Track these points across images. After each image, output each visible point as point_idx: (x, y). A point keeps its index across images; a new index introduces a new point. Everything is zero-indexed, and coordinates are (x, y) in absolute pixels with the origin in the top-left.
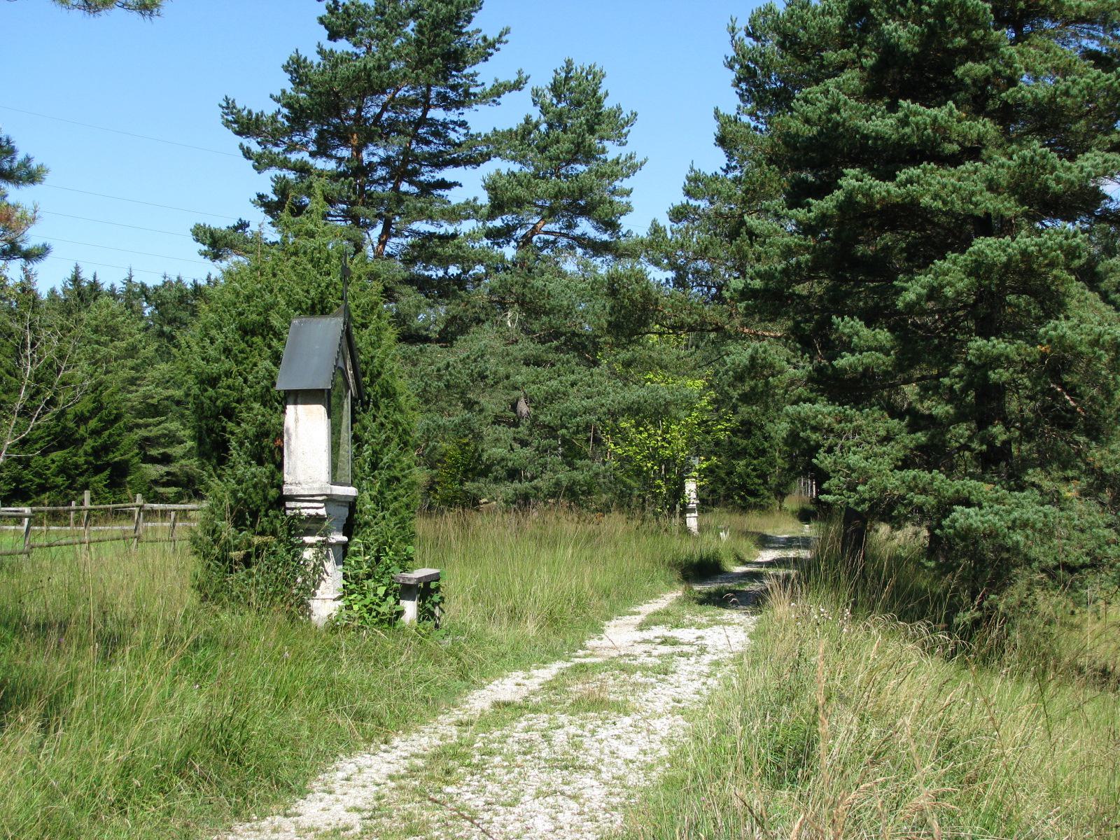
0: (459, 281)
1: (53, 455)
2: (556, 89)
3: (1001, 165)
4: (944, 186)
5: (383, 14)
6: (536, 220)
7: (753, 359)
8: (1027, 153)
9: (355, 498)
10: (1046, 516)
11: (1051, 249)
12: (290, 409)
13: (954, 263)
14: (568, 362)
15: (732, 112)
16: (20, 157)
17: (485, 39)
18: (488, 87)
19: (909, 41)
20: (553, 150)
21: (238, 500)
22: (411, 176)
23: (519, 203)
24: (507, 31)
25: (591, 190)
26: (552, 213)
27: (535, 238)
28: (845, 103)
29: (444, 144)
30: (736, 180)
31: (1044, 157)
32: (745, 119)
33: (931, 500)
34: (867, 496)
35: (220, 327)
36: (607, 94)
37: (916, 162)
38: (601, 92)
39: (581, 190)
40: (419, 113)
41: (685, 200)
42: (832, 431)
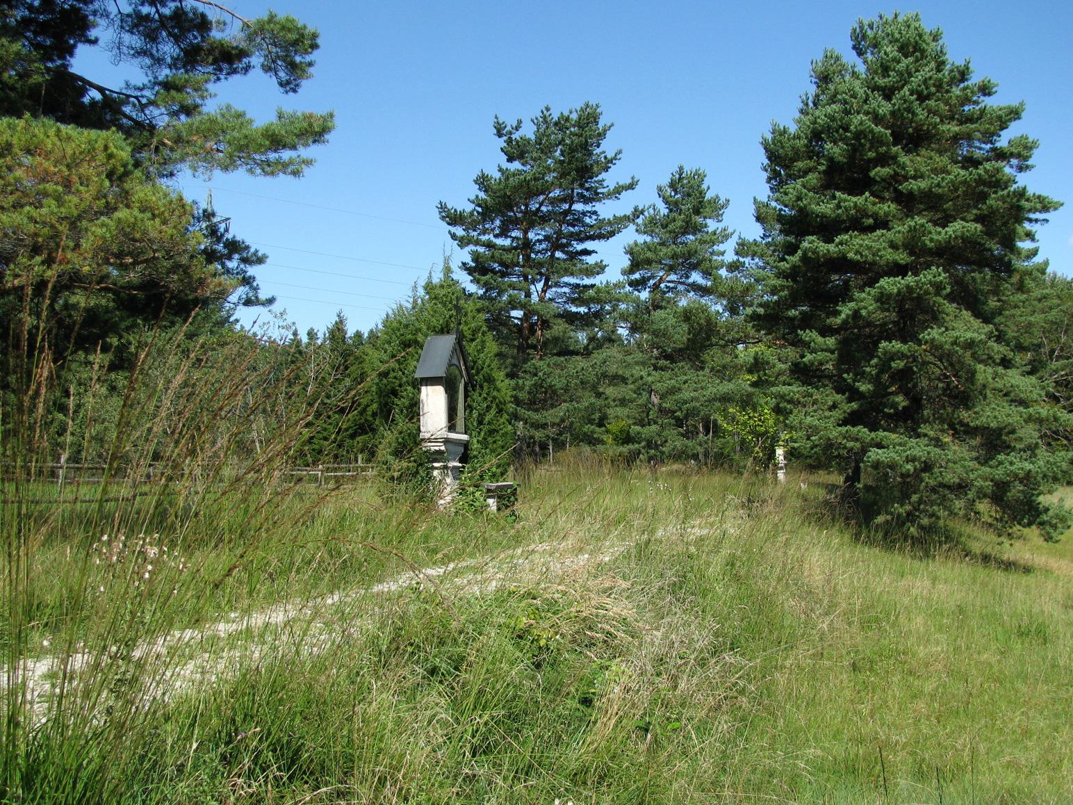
0: (597, 315)
1: (358, 439)
2: (673, 185)
3: (900, 229)
4: (861, 246)
5: (540, 144)
6: (661, 274)
7: (756, 358)
8: (913, 224)
9: (468, 442)
10: (929, 453)
11: (924, 284)
12: (423, 389)
13: (869, 294)
14: (683, 367)
15: (765, 200)
16: (252, 250)
17: (605, 157)
18: (612, 188)
19: (839, 154)
20: (671, 227)
21: (399, 444)
22: (561, 247)
23: (649, 262)
24: (620, 152)
25: (696, 252)
26: (671, 269)
27: (662, 285)
28: (806, 195)
29: (583, 226)
30: (768, 244)
31: (922, 225)
32: (774, 204)
33: (858, 445)
34: (817, 443)
35: (389, 343)
36: (709, 188)
37: (846, 231)
38: (704, 186)
39: (689, 252)
40: (566, 206)
41: (735, 258)
42: (799, 403)
